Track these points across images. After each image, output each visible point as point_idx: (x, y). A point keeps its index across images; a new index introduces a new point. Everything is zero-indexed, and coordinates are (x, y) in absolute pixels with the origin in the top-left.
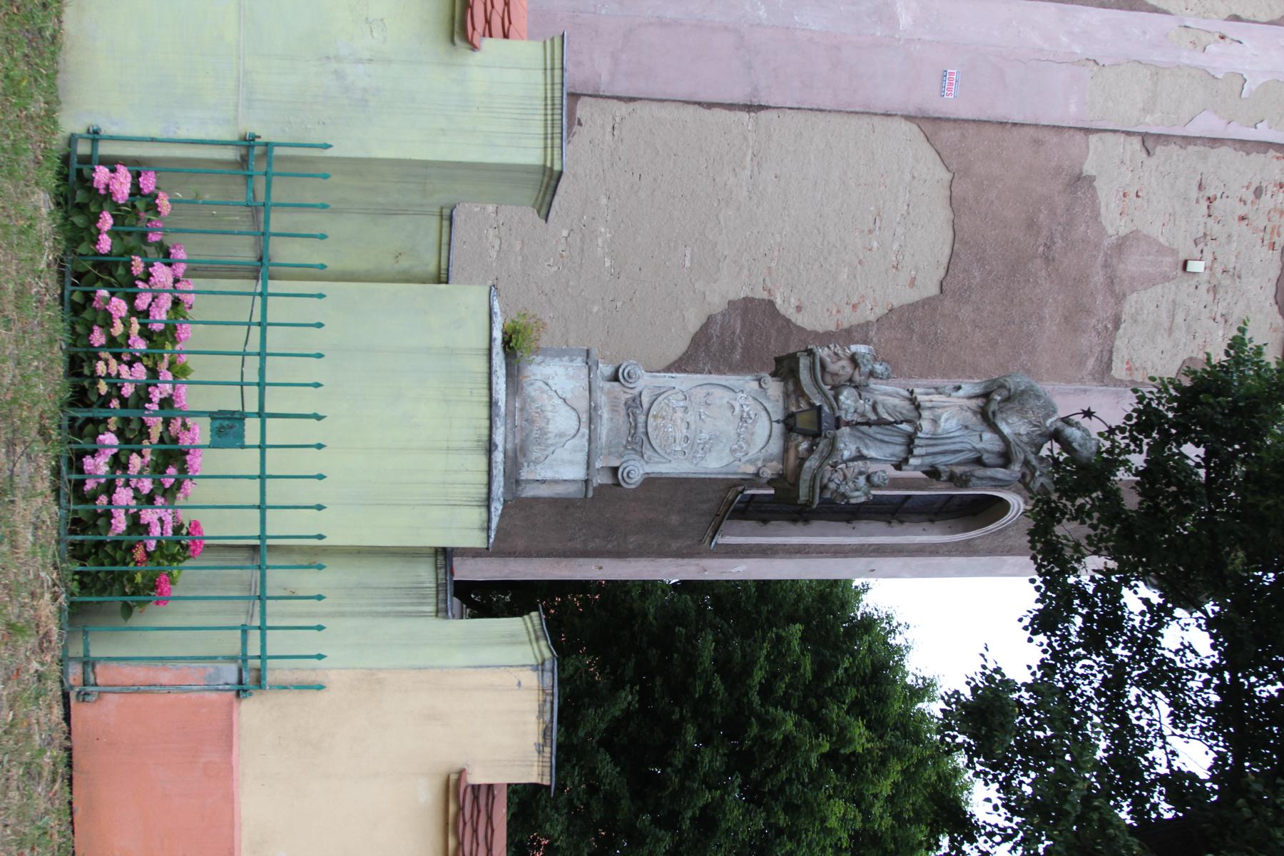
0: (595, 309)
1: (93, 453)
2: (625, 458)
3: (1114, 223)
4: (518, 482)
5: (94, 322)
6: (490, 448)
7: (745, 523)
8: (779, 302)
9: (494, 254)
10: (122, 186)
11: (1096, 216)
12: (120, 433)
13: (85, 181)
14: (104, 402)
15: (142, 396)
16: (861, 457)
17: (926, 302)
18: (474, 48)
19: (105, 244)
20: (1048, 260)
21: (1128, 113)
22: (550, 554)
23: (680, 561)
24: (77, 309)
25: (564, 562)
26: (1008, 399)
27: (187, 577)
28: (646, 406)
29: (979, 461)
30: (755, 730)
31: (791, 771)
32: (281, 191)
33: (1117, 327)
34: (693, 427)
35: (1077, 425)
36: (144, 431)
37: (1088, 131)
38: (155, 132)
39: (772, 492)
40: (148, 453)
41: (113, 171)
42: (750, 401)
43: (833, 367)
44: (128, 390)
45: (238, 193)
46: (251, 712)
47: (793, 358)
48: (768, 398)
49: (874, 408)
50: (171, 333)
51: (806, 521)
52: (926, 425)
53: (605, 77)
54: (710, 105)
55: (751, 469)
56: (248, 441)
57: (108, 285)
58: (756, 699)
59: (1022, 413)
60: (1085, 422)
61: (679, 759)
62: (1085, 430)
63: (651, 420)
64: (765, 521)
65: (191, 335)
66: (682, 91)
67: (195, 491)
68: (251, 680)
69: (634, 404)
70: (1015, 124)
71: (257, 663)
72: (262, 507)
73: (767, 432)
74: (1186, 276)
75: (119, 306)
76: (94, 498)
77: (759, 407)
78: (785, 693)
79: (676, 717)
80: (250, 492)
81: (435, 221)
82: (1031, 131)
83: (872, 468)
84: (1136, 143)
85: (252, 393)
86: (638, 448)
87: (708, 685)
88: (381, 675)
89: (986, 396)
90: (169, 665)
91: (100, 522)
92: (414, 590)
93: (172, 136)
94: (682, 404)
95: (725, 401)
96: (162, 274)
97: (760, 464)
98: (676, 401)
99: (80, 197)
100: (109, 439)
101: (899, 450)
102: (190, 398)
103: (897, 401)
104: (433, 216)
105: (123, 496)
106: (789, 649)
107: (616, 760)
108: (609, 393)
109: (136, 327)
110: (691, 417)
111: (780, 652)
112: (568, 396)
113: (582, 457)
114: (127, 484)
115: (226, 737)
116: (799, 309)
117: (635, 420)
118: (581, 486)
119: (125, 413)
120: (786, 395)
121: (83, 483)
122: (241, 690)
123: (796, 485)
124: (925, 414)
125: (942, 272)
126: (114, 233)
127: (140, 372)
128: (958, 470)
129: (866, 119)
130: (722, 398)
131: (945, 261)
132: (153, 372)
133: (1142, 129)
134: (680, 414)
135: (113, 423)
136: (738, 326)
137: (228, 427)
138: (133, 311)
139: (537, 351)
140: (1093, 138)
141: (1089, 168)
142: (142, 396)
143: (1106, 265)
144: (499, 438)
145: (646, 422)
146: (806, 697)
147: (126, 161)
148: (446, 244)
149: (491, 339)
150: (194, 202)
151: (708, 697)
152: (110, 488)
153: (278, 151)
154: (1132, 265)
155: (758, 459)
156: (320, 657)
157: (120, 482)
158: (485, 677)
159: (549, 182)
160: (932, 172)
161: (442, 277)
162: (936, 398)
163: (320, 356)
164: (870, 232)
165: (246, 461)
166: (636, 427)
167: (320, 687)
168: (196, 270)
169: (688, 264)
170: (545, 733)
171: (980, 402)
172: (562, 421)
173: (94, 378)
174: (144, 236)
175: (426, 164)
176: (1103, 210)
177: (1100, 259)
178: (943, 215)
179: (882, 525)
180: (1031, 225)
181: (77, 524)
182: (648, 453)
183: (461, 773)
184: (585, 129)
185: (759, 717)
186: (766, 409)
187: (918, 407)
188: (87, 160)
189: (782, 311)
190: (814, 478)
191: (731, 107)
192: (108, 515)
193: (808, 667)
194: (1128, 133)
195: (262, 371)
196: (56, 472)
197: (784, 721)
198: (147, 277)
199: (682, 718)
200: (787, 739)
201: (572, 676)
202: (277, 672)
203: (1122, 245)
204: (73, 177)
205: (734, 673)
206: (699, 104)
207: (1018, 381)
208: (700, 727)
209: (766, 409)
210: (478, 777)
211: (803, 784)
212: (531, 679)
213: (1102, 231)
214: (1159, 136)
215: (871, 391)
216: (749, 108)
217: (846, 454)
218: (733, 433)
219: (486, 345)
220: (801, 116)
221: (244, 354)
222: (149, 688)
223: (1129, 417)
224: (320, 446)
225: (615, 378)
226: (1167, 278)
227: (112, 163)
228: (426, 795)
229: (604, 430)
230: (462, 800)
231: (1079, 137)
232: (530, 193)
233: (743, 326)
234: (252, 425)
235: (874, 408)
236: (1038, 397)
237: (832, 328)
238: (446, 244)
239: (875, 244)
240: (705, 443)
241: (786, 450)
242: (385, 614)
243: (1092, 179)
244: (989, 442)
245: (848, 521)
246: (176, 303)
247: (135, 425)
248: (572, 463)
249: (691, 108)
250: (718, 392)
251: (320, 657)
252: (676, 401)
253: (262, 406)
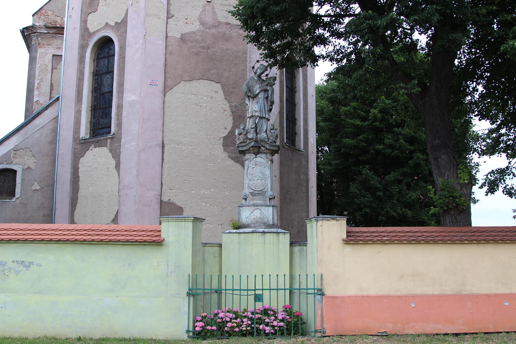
0: (227, 193)
1: (265, 330)
3: (196, 26)
4: (273, 225)
5: (233, 330)
6: (264, 232)
7: (296, 140)
8: (224, 135)
9: (211, 226)
10: (201, 324)
11: (194, 33)
12: (260, 324)
13: (199, 333)
14: (252, 328)
15: (251, 319)
16: (266, 131)
17: (223, 87)
18: (164, 240)
19: (214, 328)
20: (208, 48)
21: (159, 24)
22: (308, 204)
23: (310, 161)
24: (230, 335)
25: (310, 199)
26: (250, 91)
27: (295, 309)
28: (253, 191)
29: (267, 98)
30: (377, 123)
31: (393, 110)
32: (200, 286)
33: (229, 24)
35: (257, 70)
36: (259, 319)
37: (167, 37)
38: (187, 317)
40: (264, 318)
41: (197, 326)
43: (242, 140)
44: (249, 322)
45: (200, 297)
46: (328, 292)
47: (240, 151)
49: (253, 128)
50: (235, 313)
51: (295, 120)
52: (257, 114)
53: (155, 193)
54: (163, 159)
56: (261, 293)
57: (224, 328)
58: (367, 123)
59: (253, 86)
60: (256, 68)
61: (388, 151)
62: (258, 68)
64: (296, 133)
65: (236, 308)
66: (158, 168)
67: (274, 306)
68: (321, 292)
69: (252, 194)
70: (165, 61)
71: (316, 291)
72: (277, 290)
75: (229, 324)
76: (276, 330)
78: (364, 112)
79: (373, 151)
80: (274, 293)
81: (206, 248)
82: (167, 55)
83: (269, 128)
84: (170, 20)
85: (250, 293)
87: (362, 141)
88: (319, 260)
89: (249, 97)
90: (316, 312)
91: (281, 329)
92: (301, 251)
93: (187, 313)
96: (221, 315)
98: (251, 183)
99: (203, 334)
100: (261, 327)
101: (264, 121)
102: (251, 308)
103: (251, 122)
104: (206, 248)
105: (275, 323)
106: (349, 111)
107: (389, 173)
109: (234, 320)
110: (256, 179)
111: (350, 114)
112: (250, 212)
113: (266, 208)
114: (272, 322)
115: (334, 298)
116: (226, 129)
118: (274, 208)
119: (255, 323)
120: (249, 153)
121: (272, 333)
122: (323, 294)
123: (273, 150)
124: (254, 114)
125: (213, 83)
126: (212, 326)
127: (245, 320)
128: (269, 104)
129: (165, 109)
131: (209, 82)
132: (245, 317)
133: (166, 19)
134: (255, 182)
135: (257, 326)
136: (232, 148)
137: (258, 298)
138: (230, 321)
139: (239, 220)
140: (169, 35)
141: (179, 36)
142: (251, 319)
143: (209, 29)
144: (261, 230)
146: (366, 104)
147: (194, 324)
148: (212, 245)
149: (236, 233)
150: (203, 307)
151: (366, 140)
152: (273, 327)
153: (191, 287)
154: (209, 20)
156: (314, 275)
157: (272, 324)
158: (319, 235)
159: (197, 220)
160: (182, 87)
161: (220, 246)
162: (250, 111)
163: (240, 276)
164: (201, 106)
165: (266, 293)
167: (322, 275)
168: (220, 307)
169: (212, 165)
170: (333, 219)
171: (250, 98)
172: (257, 213)
173: (246, 330)
174: (212, 319)
175: (193, 251)
176: (192, 30)
177: (208, 30)
178: (195, 83)
179: (297, 94)
180: (197, 54)
181: (282, 334)
182: (265, 190)
183: (343, 240)
184: (171, 198)
185: (373, 122)
187: (252, 116)
188: (194, 333)
189: (227, 134)
190: (271, 146)
191: (163, 153)
192: (280, 327)
193: (355, 104)
194: (167, 23)
195: (244, 290)
196: (269, 339)
197: (374, 113)
198: (222, 318)
199: (374, 149)
200: (381, 112)
201: (358, 189)
202: (318, 286)
203: (203, 24)
204: (198, 336)
205: (358, 131)
206: (162, 163)
207: (244, 88)
208: (377, 143)
210: (345, 236)
211: (398, 105)
212: (320, 223)
213: (199, 30)
214: (167, 13)
215: (248, 129)
216: (163, 147)
217: (265, 136)
219: (237, 234)
220: (165, 130)
221: (240, 295)
222: (322, 316)
223: (255, 45)
224: (262, 276)
226: (213, 8)
227: (194, 327)
228: (349, 249)
229: (259, 202)
230: (351, 239)
231: (169, 40)
232: (199, 224)
233: (231, 146)
234: (258, 292)
235: (253, 128)
236: (249, 82)
237: (232, 118)
238: (212, 245)
239: (205, 105)
241: (264, 153)
242: (306, 259)
243: (182, 35)
244: (261, 96)
245: (295, 105)
246: (228, 312)
247: (258, 321)
248: (268, 211)
249: (164, 165)
250: (249, 171)
251: (314, 275)
252: (251, 183)
253: (253, 290)
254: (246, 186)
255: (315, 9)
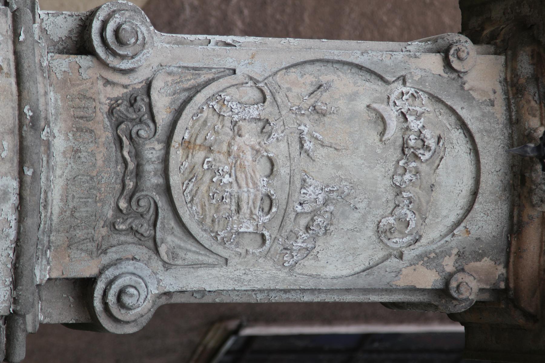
2: (112, 255)
28: (163, 116)
34: (283, 171)
39: (460, 328)
42: (425, 105)
48: (466, 96)
55: (429, 279)
63: (177, 155)
73: (467, 183)
74: (465, 62)
77: (448, 120)
86: (145, 229)
94: (254, 112)
95: (361, 105)
97: (449, 264)
108: (65, 83)
110: (278, 149)
117: (137, 155)
130: (353, 97)
134: (249, 137)
145: (165, 160)
155: (446, 253)
166: (138, 173)
182: (170, 239)
186: (463, 125)
209: (463, 125)
218: (383, 186)
225: (80, 44)
240: (315, 213)
241: (515, 228)
250: (343, 83)
252: (240, 99)
254: (201, 50)
255: (460, 328)
